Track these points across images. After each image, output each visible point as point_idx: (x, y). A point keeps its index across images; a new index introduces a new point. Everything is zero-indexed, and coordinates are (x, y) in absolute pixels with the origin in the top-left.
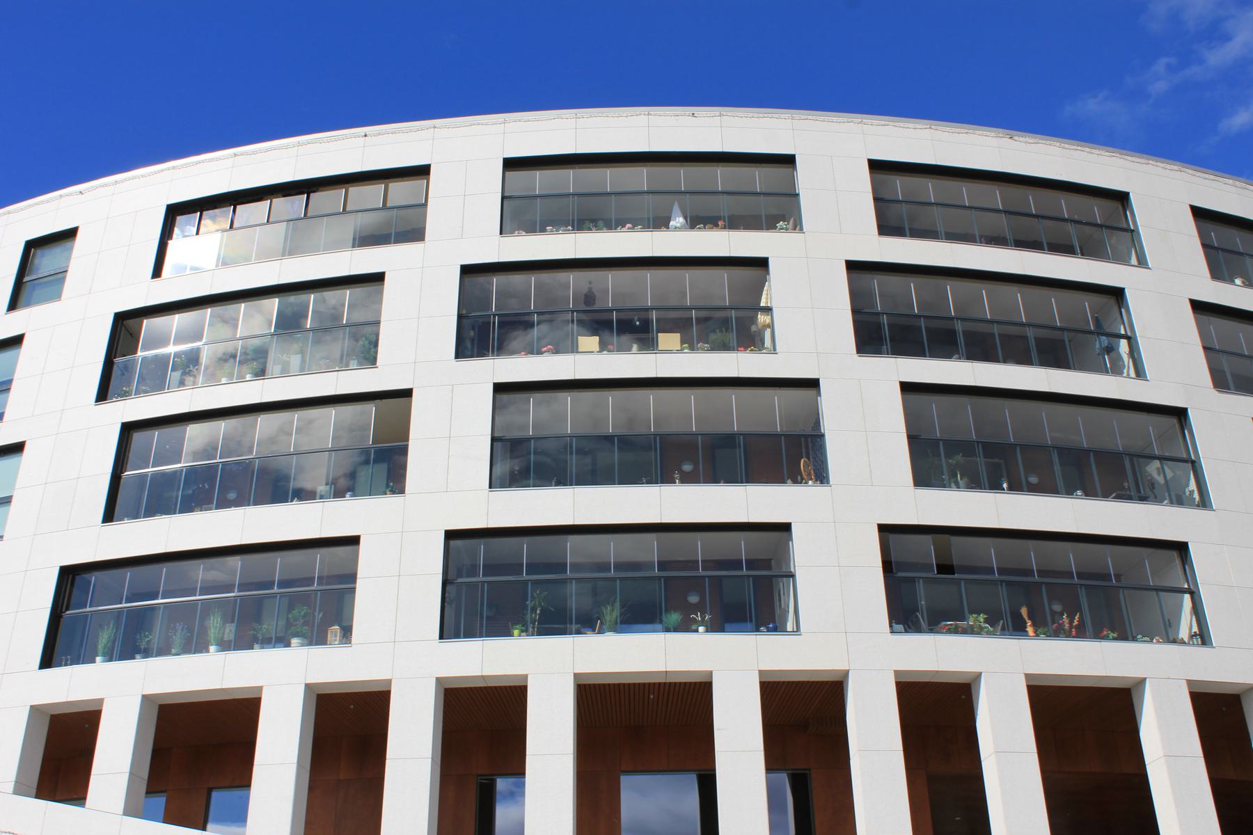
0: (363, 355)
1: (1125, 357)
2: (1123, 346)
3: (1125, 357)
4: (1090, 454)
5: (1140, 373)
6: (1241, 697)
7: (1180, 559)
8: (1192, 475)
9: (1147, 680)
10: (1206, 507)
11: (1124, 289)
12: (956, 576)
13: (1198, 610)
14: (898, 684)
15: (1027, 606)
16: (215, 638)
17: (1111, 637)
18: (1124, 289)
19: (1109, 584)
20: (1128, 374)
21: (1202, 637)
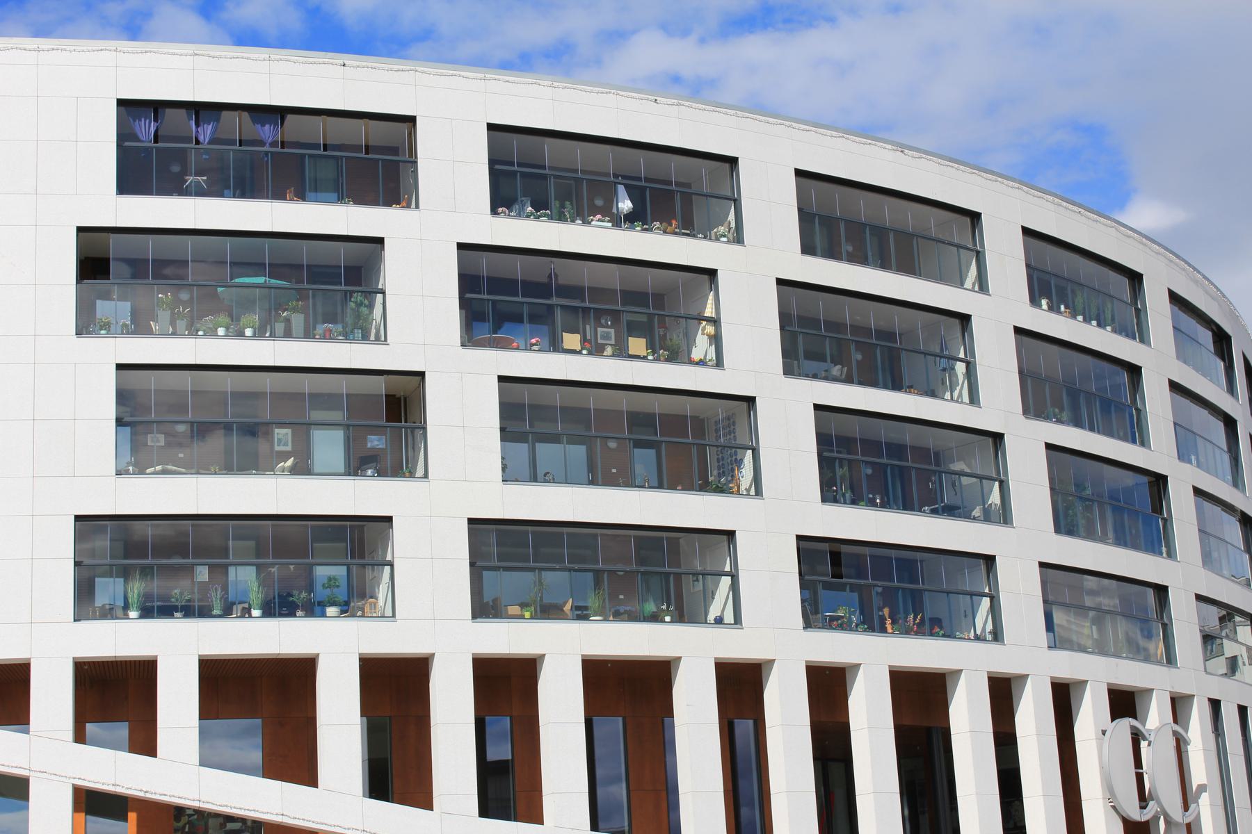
0: (315, 332)
1: (961, 377)
2: (960, 368)
3: (961, 377)
4: (583, 182)
5: (974, 399)
6: (1135, 694)
7: (985, 566)
8: (733, 207)
9: (1089, 682)
10: (1171, 664)
11: (971, 316)
12: (844, 580)
13: (995, 610)
14: (807, 666)
15: (889, 608)
16: (139, 593)
17: (941, 634)
18: (971, 316)
19: (186, 283)
20: (960, 395)
21: (997, 635)
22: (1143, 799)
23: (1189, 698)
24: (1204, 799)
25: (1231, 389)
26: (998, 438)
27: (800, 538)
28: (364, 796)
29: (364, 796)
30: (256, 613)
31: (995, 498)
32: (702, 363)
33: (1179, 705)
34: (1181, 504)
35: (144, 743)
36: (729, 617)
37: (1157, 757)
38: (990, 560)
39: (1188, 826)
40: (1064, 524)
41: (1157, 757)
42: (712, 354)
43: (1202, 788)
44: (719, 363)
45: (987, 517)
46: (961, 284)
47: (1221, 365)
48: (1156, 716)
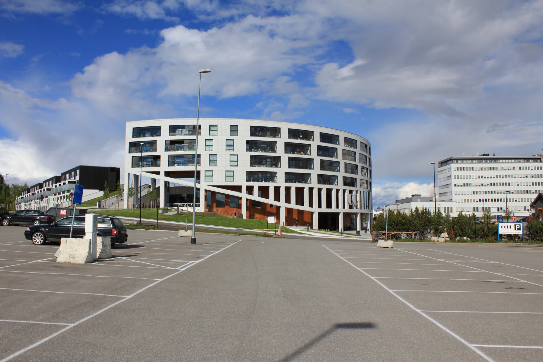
2: (336, 154)
5: (337, 158)
13: (337, 182)
21: (337, 185)
22: (352, 202)
23: (358, 191)
24: (358, 202)
25: (367, 153)
26: (339, 162)
27: (288, 129)
28: (246, 194)
29: (246, 194)
30: (263, 181)
31: (338, 169)
32: (308, 155)
33: (357, 192)
34: (359, 168)
35: (303, 205)
36: (310, 183)
37: (354, 198)
38: (337, 176)
39: (356, 206)
40: (346, 171)
41: (354, 198)
42: (310, 154)
43: (358, 201)
44: (310, 155)
45: (337, 171)
46: (336, 144)
47: (366, 149)
48: (354, 193)
